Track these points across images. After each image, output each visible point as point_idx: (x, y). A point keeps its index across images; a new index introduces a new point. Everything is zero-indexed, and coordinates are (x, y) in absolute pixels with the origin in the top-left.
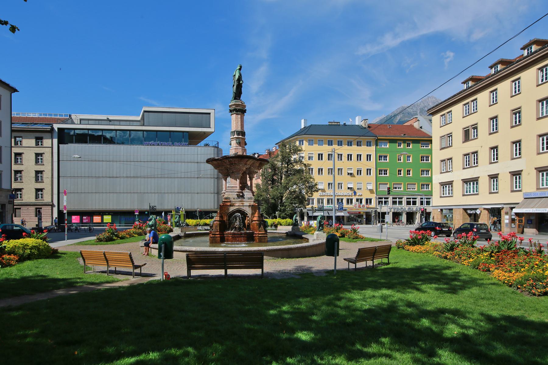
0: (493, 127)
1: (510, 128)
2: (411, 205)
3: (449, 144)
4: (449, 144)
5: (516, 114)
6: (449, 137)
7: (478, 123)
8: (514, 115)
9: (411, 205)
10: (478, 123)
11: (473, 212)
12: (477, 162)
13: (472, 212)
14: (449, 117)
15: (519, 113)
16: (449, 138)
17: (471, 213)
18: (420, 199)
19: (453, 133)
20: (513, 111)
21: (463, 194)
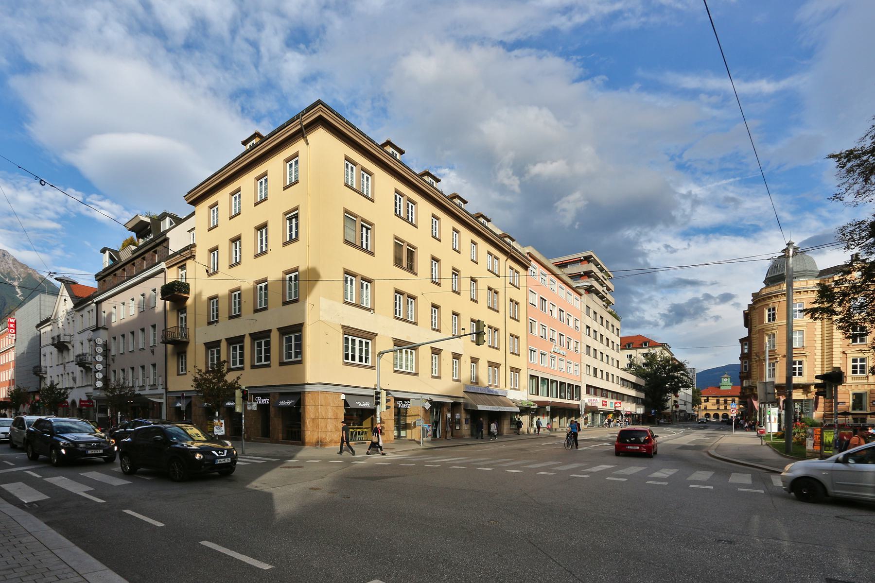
0: (262, 239)
1: (228, 267)
2: (857, 342)
3: (236, 258)
4: (236, 258)
5: (290, 219)
6: (290, 219)
7: (218, 246)
8: (288, 221)
9: (857, 342)
10: (218, 246)
11: (265, 400)
12: (217, 315)
13: (263, 401)
14: (214, 216)
15: (296, 217)
16: (291, 223)
17: (263, 403)
18: (245, 369)
19: (300, 209)
20: (286, 215)
21: (281, 361)
